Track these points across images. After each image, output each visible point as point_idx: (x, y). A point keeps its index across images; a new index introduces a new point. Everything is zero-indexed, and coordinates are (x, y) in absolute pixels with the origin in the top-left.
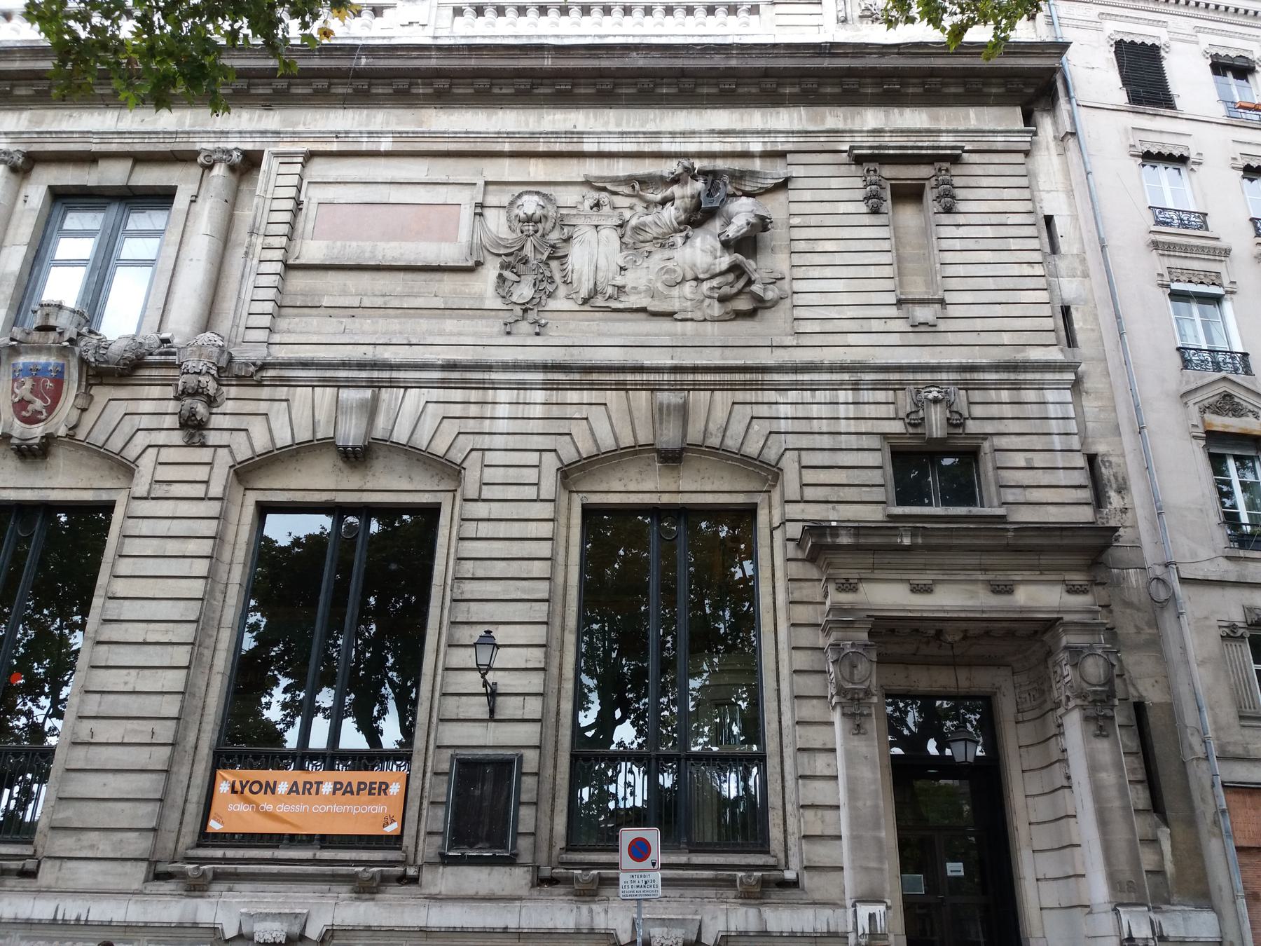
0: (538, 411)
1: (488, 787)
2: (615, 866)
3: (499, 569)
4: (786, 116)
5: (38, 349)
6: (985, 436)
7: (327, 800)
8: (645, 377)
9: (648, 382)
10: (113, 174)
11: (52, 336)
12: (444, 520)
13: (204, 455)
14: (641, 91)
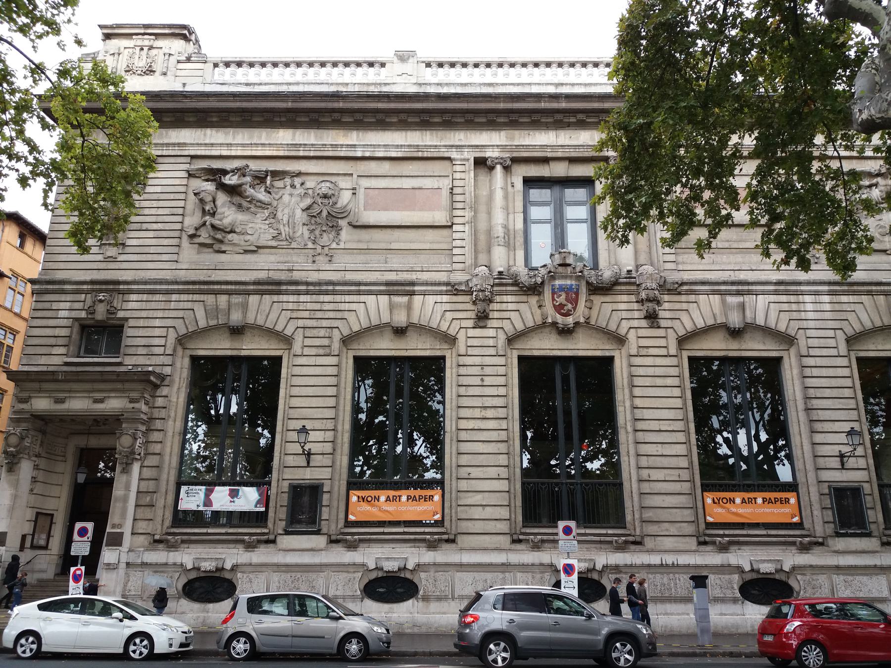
0: (828, 307)
1: (850, 501)
2: (557, 534)
3: (827, 393)
4: (312, 134)
5: (565, 277)
6: (126, 319)
7: (760, 506)
8: (882, 288)
9: (884, 291)
10: (559, 170)
11: (569, 269)
12: (448, 364)
13: (661, 332)
14: (311, 120)
